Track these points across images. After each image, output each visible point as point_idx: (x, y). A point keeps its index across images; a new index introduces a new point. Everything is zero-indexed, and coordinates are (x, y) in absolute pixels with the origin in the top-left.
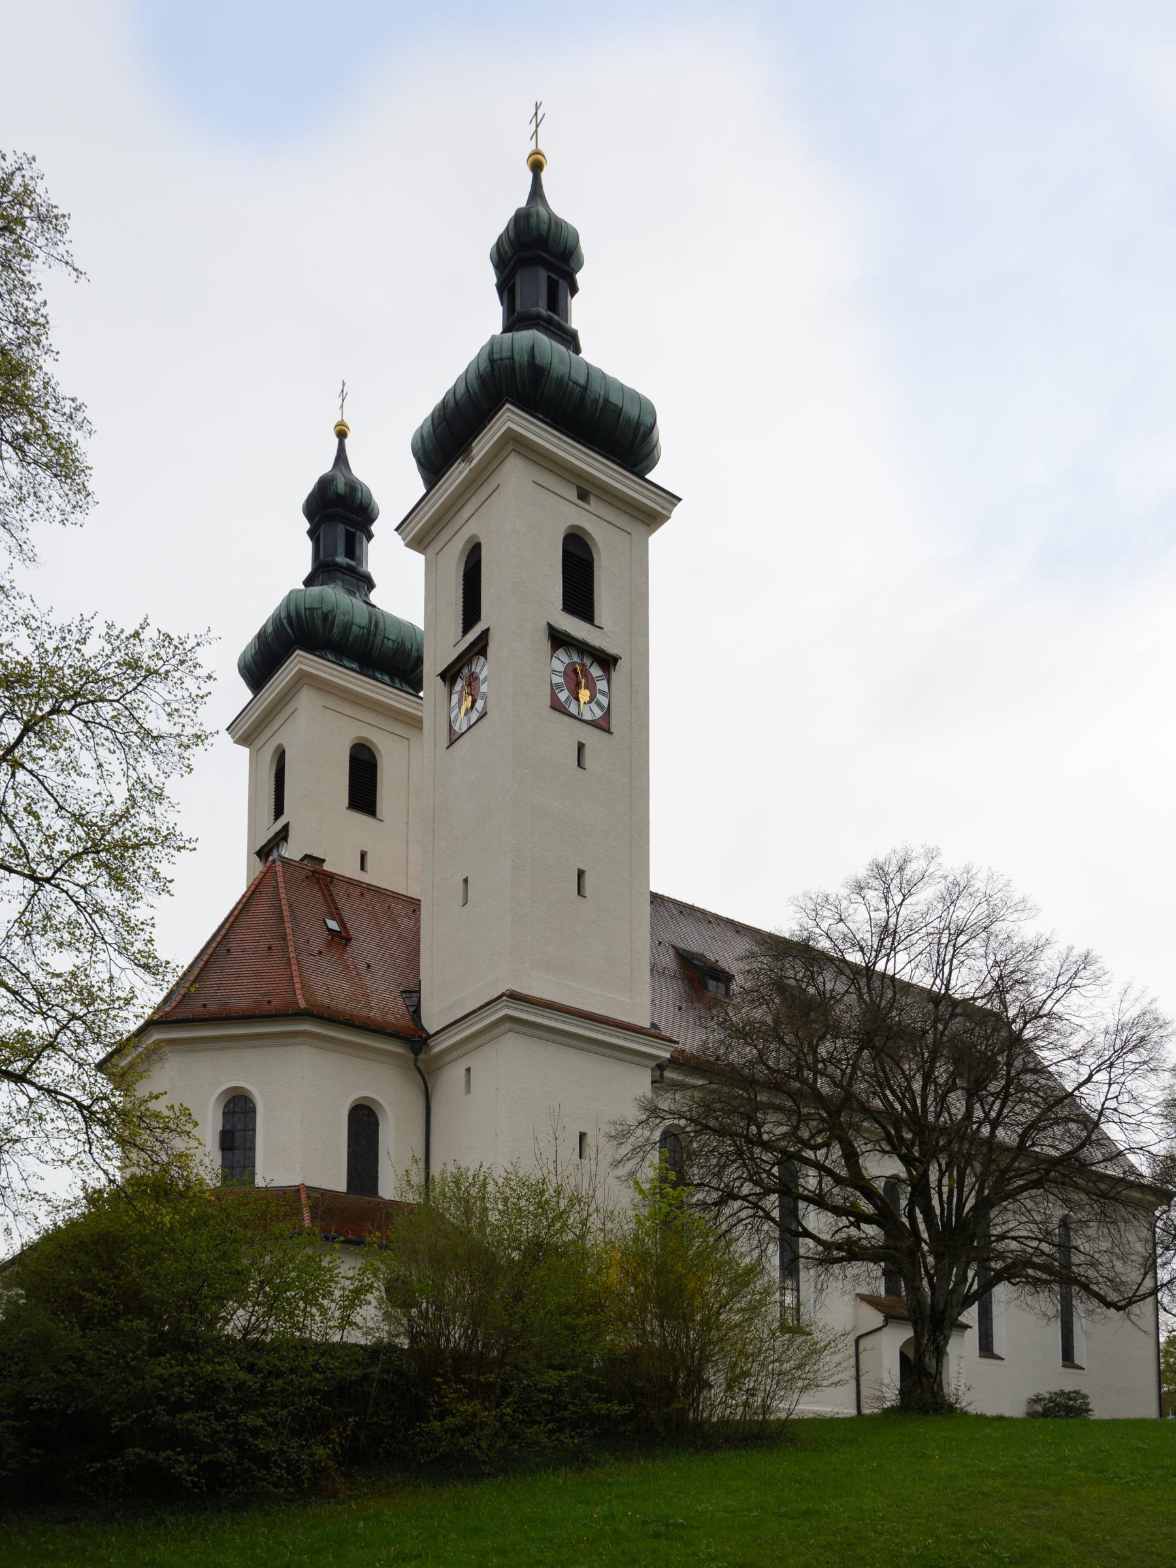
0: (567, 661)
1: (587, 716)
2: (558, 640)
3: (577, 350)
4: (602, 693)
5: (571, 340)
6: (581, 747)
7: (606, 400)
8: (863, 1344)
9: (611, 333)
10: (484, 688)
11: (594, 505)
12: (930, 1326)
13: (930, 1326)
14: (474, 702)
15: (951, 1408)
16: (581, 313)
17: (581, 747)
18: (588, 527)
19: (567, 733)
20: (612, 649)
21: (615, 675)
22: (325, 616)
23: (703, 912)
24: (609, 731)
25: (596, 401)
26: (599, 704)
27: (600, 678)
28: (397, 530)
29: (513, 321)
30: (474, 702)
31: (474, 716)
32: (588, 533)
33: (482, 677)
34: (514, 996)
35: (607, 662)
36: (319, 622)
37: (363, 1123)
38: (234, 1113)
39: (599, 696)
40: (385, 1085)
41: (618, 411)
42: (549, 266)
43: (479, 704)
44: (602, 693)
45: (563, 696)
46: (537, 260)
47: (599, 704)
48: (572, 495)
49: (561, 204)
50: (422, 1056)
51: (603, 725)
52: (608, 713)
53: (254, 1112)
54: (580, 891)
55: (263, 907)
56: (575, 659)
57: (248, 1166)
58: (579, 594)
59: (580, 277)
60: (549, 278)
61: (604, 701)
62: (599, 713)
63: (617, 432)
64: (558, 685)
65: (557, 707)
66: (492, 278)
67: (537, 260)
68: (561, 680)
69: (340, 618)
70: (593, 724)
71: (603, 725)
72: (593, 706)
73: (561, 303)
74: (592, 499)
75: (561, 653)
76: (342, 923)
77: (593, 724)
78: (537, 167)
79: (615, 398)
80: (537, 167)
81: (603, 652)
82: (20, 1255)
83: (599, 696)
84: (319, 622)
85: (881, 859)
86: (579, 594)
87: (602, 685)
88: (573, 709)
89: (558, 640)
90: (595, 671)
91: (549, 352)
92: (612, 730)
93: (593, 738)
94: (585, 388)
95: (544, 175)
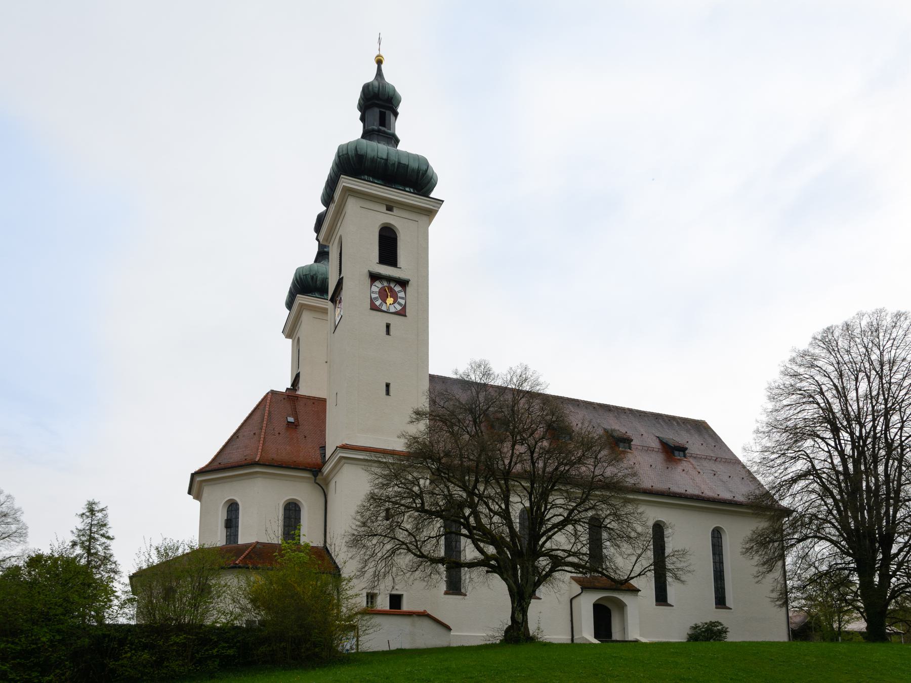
0: (380, 286)
1: (392, 310)
4: (401, 298)
6: (388, 326)
7: (399, 163)
8: (574, 601)
9: (412, 136)
11: (396, 211)
12: (521, 597)
13: (521, 597)
15: (531, 639)
16: (401, 126)
17: (388, 326)
18: (392, 222)
19: (380, 320)
21: (408, 289)
22: (312, 277)
23: (630, 410)
25: (394, 164)
26: (400, 304)
27: (400, 292)
29: (366, 134)
34: (345, 447)
35: (404, 284)
36: (310, 280)
37: (292, 512)
38: (290, 510)
40: (300, 490)
41: (406, 167)
44: (401, 298)
45: (378, 303)
46: (379, 104)
47: (400, 304)
48: (384, 209)
49: (390, 78)
50: (319, 477)
51: (402, 313)
52: (404, 307)
53: (238, 509)
55: (259, 413)
57: (236, 535)
59: (399, 110)
61: (402, 302)
63: (416, 179)
64: (376, 298)
65: (374, 308)
67: (379, 104)
69: (320, 277)
70: (397, 313)
71: (402, 313)
72: (396, 305)
73: (387, 122)
74: (395, 209)
76: (296, 419)
77: (397, 313)
78: (379, 62)
79: (404, 161)
80: (379, 62)
81: (399, 279)
84: (310, 280)
85: (767, 386)
87: (402, 294)
88: (384, 308)
90: (397, 288)
93: (395, 321)
94: (387, 160)
95: (383, 66)
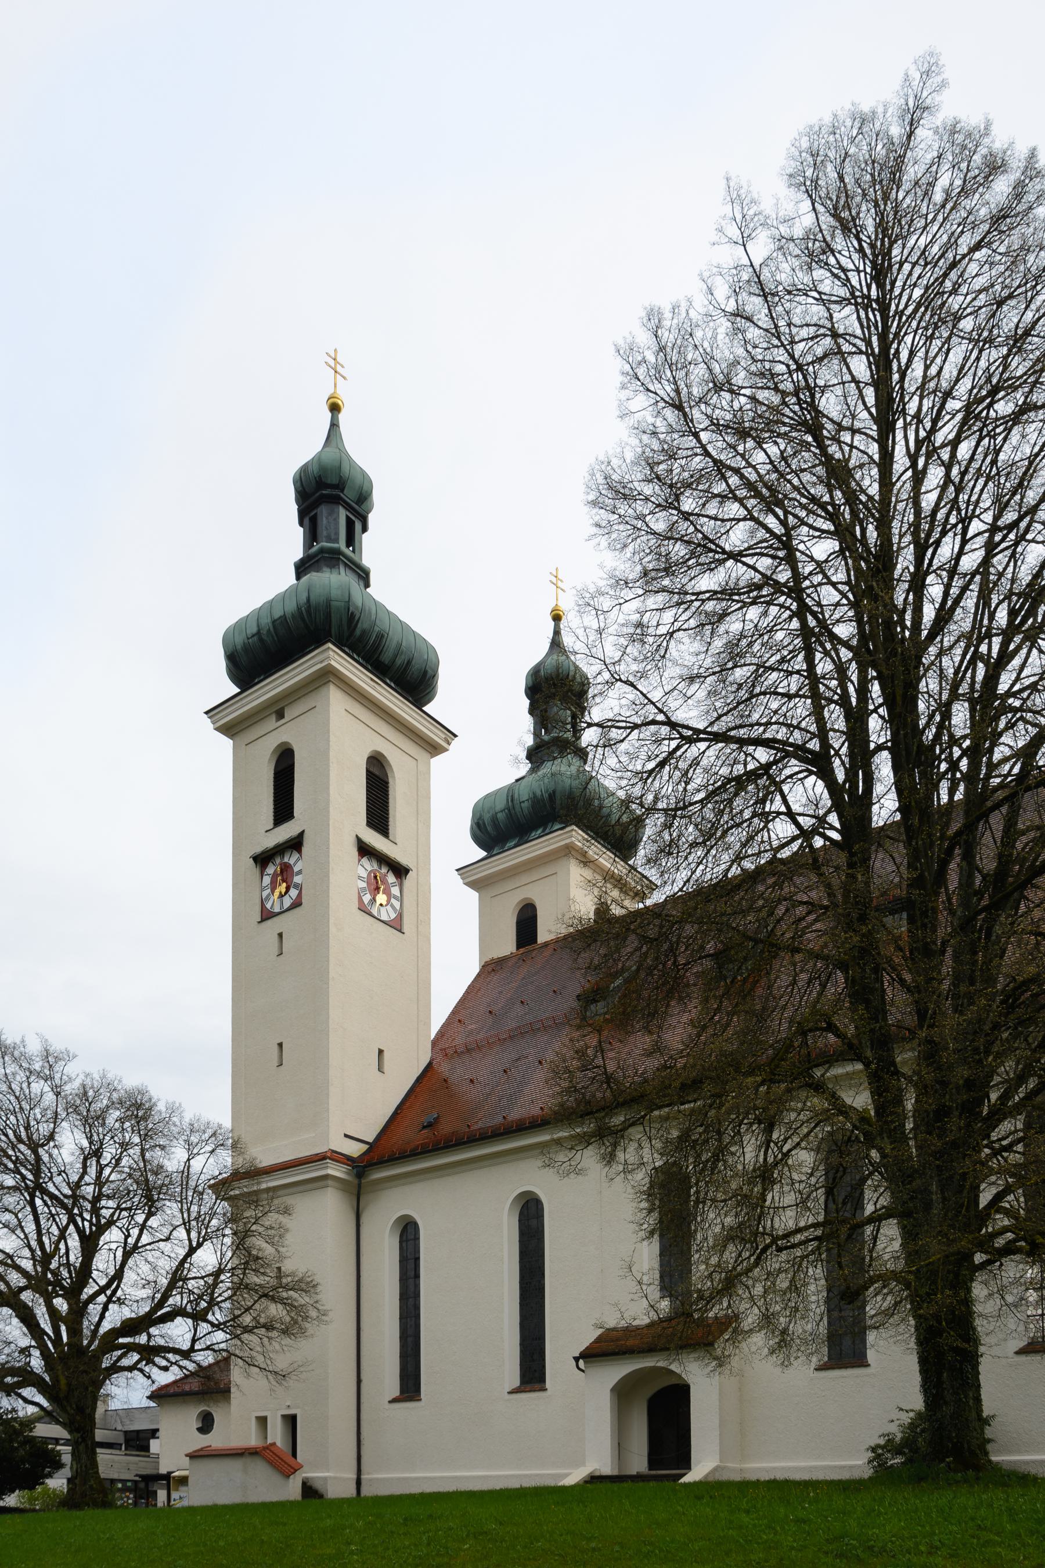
0: (369, 868)
1: (384, 917)
2: (365, 850)
3: (367, 585)
4: (395, 897)
5: (364, 576)
10: (297, 879)
14: (288, 889)
16: (372, 549)
20: (403, 860)
24: (400, 931)
28: (206, 713)
30: (288, 889)
31: (287, 902)
32: (390, 765)
33: (296, 869)
35: (400, 871)
39: (393, 901)
42: (348, 507)
43: (293, 893)
44: (395, 897)
46: (330, 499)
51: (397, 925)
52: (400, 916)
54: (380, 1069)
56: (376, 866)
58: (378, 815)
60: (347, 517)
62: (393, 916)
65: (363, 909)
66: (294, 508)
67: (330, 499)
68: (365, 885)
71: (397, 925)
75: (365, 861)
82: (971, 1323)
83: (393, 901)
86: (378, 815)
89: (365, 850)
90: (391, 878)
91: (360, 605)
92: (405, 929)
